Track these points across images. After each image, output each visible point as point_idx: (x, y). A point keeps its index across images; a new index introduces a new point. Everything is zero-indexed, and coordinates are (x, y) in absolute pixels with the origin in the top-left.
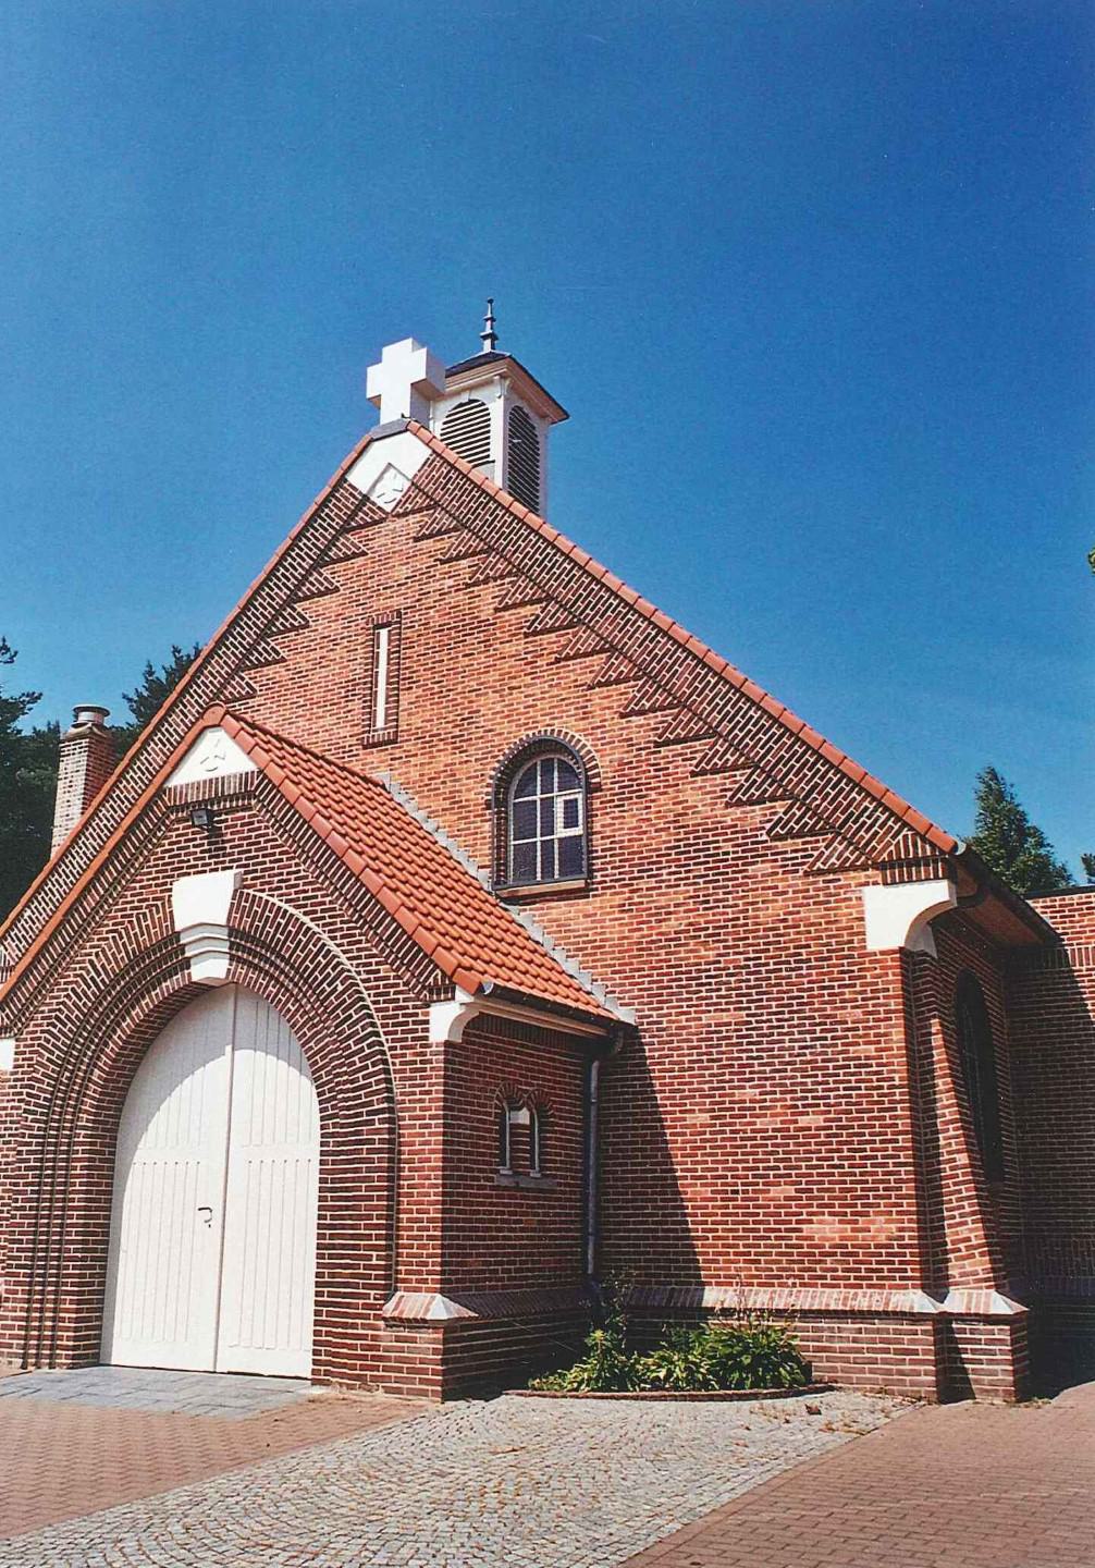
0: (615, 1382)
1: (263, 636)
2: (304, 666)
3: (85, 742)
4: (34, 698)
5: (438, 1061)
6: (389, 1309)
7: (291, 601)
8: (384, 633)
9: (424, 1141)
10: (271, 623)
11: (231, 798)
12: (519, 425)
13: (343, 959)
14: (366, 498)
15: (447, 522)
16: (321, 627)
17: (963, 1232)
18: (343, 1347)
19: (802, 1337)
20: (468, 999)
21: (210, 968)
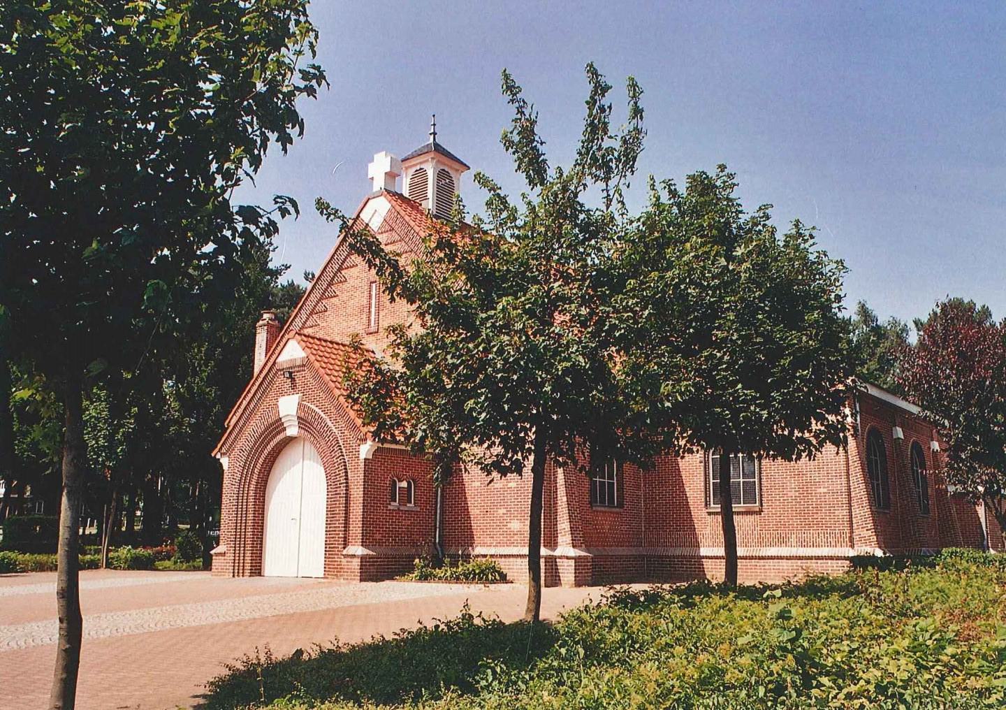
0: (424, 578)
1: (330, 285)
2: (345, 299)
3: (266, 328)
4: (287, 267)
5: (362, 465)
6: (345, 552)
7: (340, 270)
8: (374, 285)
9: (357, 493)
10: (333, 279)
11: (299, 366)
12: (442, 175)
13: (333, 428)
14: (367, 225)
15: (397, 238)
16: (351, 282)
17: (563, 526)
18: (332, 567)
19: (503, 565)
20: (371, 443)
21: (292, 431)
